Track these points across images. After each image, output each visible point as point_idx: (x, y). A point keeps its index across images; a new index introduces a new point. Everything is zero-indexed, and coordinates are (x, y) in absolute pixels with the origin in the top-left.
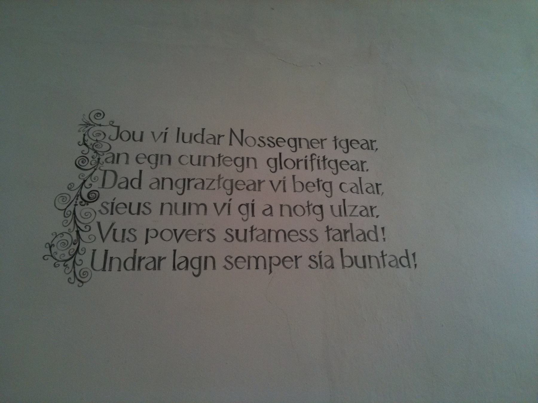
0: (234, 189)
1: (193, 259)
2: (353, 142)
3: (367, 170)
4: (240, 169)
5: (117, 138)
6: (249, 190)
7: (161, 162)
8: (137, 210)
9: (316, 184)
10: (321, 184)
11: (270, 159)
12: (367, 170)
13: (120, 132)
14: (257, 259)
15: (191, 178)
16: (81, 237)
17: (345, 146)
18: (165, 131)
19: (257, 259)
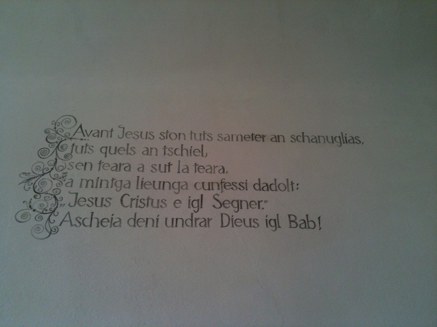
0: (123, 187)
1: (194, 200)
2: (226, 202)
3: (263, 209)
4: (236, 209)
5: (75, 204)
6: (67, 186)
7: (157, 225)
8: (165, 185)
9: (251, 137)
10: (254, 136)
11: (314, 228)
12: (263, 209)
13: (78, 199)
14: (88, 181)
15: (260, 200)
16: (59, 155)
17: (236, 206)
18: (137, 198)
19: (88, 181)
